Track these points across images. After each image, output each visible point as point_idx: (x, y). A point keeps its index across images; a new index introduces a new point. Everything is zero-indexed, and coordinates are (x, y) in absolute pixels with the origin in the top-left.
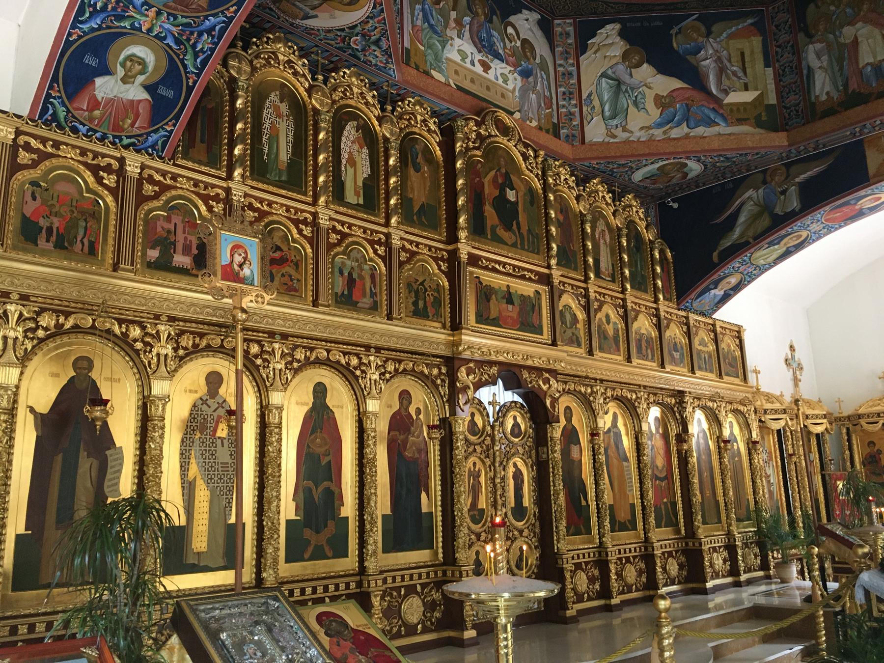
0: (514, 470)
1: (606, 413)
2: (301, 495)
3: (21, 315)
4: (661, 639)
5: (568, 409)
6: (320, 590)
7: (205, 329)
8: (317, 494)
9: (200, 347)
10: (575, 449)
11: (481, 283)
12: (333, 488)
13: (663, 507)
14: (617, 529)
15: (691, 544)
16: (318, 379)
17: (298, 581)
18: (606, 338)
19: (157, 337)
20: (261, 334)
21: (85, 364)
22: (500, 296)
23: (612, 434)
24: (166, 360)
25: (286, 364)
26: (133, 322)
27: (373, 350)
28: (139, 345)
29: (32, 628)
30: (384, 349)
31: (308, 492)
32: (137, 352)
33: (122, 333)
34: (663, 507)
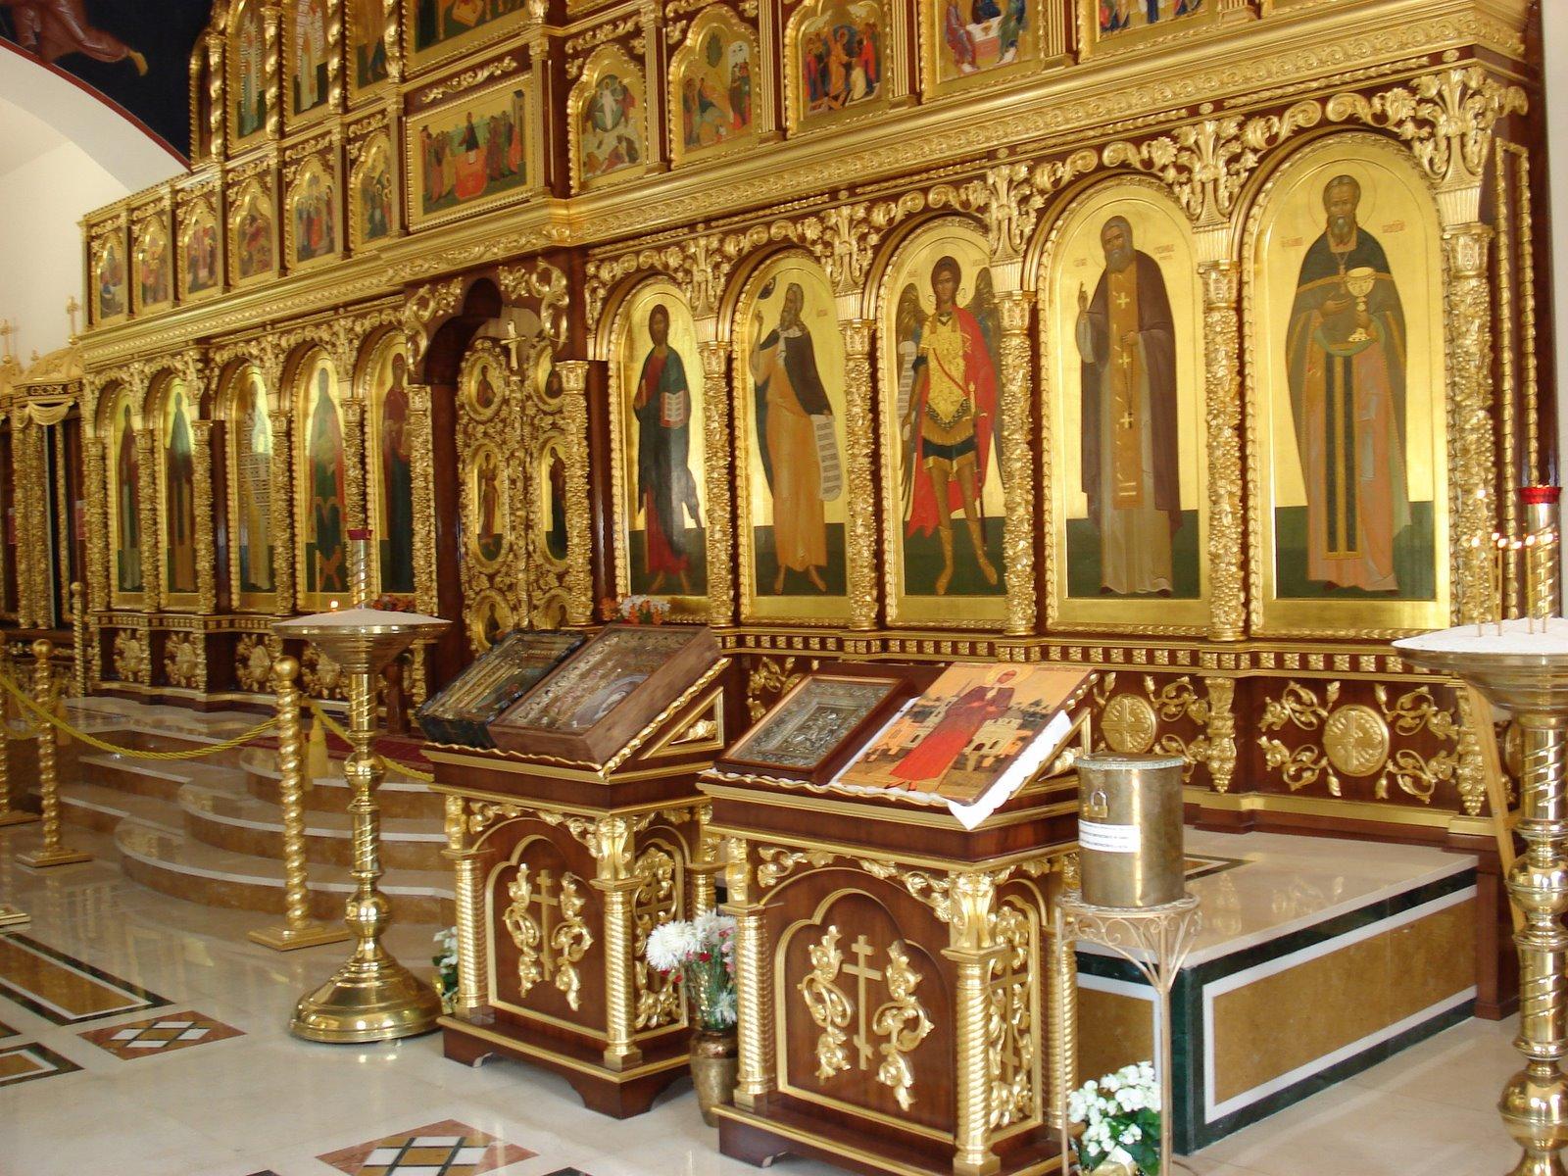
0: (551, 461)
1: (766, 293)
2: (314, 514)
3: (1465, 87)
4: (300, 786)
5: (179, 394)
6: (781, 642)
7: (258, 332)
8: (326, 512)
9: (1282, 138)
10: (672, 403)
11: (429, 136)
12: (318, 499)
13: (946, 534)
14: (779, 585)
15: (225, 624)
16: (1106, 215)
17: (800, 626)
18: (705, 105)
19: (835, 229)
20: (917, 178)
21: (1344, 191)
22: (457, 140)
23: (781, 345)
24: (1463, 146)
25: (1228, 162)
26: (1154, 136)
27: (843, 195)
28: (1409, 130)
29: (1128, 655)
30: (717, 219)
31: (319, 508)
32: (1408, 144)
33: (1143, 162)
34: (946, 534)
